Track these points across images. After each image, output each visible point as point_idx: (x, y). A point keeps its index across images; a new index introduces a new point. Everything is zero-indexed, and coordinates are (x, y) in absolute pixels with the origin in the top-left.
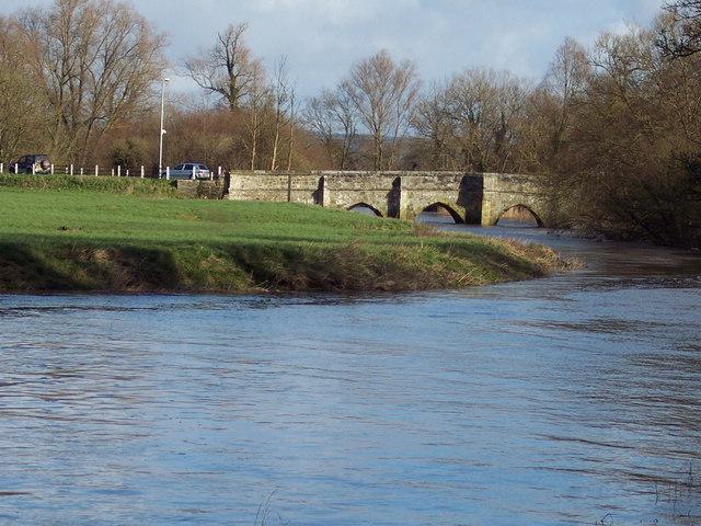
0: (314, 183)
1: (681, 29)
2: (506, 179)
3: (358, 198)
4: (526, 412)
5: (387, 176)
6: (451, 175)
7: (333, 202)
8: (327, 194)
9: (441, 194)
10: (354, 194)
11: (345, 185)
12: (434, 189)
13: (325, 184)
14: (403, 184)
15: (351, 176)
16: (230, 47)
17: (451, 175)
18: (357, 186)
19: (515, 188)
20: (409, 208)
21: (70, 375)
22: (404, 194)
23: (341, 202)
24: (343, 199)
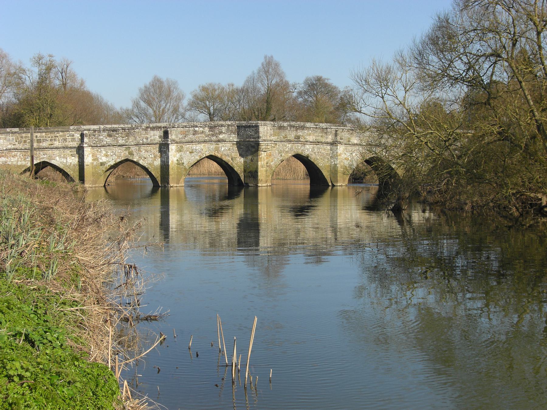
0: (73, 140)
1: (412, 314)
2: (280, 128)
3: (119, 155)
4: (266, 104)
5: (153, 129)
6: (222, 126)
7: (95, 159)
8: (88, 152)
9: (213, 146)
10: (117, 150)
11: (109, 140)
12: (205, 142)
13: (86, 140)
14: (172, 136)
15: (114, 130)
16: (64, 74)
17: (222, 126)
18: (121, 142)
19: (292, 135)
20: (180, 163)
21: (195, 242)
22: (173, 148)
23: (104, 159)
24: (107, 156)
